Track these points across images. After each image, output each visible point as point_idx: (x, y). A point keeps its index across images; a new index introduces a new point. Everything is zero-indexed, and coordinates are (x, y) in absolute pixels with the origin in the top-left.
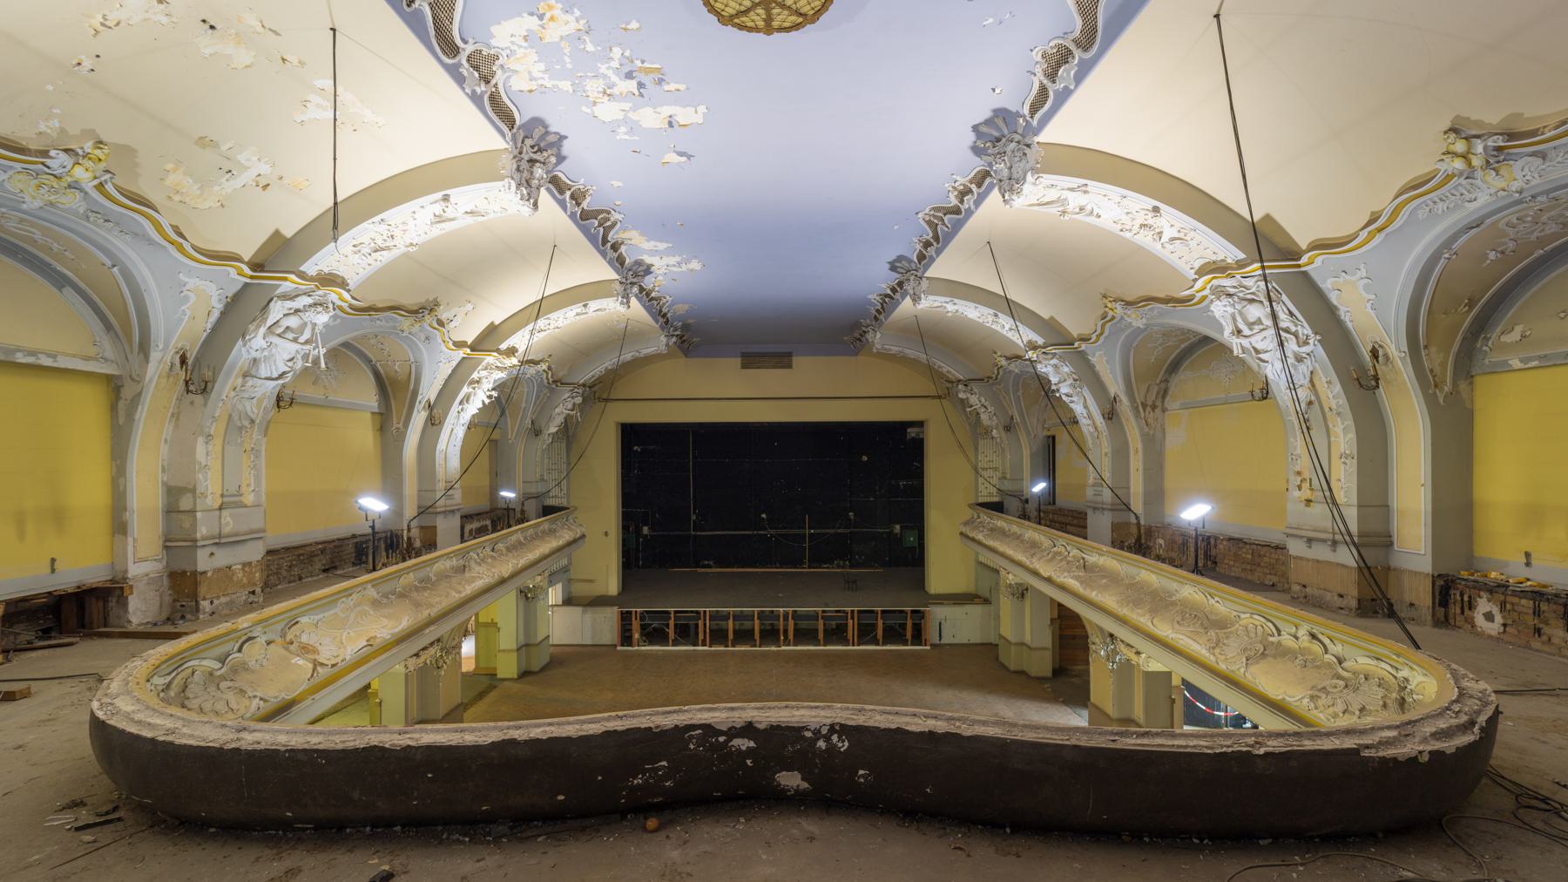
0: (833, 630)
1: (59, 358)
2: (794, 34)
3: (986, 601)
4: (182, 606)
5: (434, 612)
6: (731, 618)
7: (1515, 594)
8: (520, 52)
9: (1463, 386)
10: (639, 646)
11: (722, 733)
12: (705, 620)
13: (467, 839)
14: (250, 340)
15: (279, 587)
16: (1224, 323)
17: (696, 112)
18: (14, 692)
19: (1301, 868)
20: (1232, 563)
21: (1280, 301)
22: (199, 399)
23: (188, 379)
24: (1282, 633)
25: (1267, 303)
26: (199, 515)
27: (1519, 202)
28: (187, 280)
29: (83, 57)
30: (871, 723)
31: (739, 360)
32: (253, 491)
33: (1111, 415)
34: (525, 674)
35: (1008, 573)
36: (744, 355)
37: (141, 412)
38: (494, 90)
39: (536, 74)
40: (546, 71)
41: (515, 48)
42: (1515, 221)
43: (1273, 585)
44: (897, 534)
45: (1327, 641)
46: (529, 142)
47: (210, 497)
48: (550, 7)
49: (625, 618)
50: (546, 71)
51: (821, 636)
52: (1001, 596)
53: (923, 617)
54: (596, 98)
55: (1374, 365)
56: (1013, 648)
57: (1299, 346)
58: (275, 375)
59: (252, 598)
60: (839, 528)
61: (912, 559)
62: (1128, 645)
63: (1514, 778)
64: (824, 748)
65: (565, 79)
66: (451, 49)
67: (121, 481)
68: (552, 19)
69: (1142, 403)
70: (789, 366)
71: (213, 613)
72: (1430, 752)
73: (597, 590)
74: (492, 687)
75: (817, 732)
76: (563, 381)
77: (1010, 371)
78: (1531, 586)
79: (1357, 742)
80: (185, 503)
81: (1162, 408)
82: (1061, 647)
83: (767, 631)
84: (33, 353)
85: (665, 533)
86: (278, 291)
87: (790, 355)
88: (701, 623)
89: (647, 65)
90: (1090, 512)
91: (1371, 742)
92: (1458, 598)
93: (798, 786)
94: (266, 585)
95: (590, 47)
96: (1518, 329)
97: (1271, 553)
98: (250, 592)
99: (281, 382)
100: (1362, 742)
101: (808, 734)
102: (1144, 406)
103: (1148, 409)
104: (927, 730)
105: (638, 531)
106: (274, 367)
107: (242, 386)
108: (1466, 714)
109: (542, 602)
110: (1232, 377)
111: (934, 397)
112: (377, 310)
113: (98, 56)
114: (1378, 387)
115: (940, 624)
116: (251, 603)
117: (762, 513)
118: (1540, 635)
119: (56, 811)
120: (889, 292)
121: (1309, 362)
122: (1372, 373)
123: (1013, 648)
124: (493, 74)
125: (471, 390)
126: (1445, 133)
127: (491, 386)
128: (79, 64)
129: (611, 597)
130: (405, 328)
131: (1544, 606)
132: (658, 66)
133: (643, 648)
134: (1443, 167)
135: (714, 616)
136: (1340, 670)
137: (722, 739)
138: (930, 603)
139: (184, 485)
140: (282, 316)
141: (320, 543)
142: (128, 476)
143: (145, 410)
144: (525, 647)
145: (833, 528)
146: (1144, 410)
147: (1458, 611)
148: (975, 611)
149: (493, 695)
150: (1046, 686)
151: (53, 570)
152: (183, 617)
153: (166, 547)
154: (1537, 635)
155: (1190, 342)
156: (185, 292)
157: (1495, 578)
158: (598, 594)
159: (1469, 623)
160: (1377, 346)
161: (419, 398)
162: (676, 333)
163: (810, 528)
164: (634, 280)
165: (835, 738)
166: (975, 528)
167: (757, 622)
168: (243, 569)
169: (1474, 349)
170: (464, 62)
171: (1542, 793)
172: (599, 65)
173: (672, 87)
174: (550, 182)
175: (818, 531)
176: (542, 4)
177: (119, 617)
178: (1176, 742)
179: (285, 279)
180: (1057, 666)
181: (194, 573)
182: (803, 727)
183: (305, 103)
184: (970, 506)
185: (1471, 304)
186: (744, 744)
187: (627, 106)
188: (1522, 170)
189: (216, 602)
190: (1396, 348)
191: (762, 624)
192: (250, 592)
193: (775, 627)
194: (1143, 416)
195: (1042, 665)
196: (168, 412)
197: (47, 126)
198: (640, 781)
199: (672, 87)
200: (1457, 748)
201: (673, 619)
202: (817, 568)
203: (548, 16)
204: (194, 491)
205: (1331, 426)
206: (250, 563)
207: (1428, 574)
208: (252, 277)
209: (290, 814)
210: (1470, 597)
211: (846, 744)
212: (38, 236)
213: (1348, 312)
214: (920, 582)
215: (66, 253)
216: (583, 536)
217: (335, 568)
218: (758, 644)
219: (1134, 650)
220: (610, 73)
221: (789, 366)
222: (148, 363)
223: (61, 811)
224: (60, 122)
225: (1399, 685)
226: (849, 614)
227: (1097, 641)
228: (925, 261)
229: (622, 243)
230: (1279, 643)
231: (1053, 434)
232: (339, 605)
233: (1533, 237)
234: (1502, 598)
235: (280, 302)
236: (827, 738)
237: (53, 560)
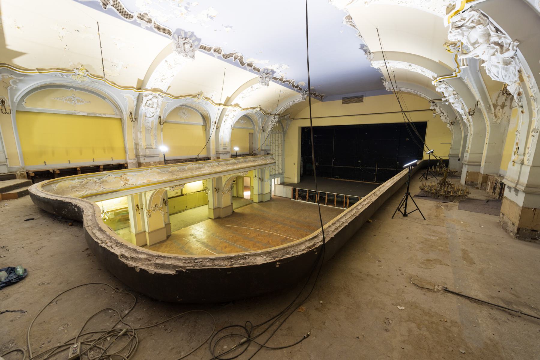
5: (178, 177)
10: (298, 200)
26: (140, 150)
28: (123, 94)
32: (155, 145)
34: (261, 202)
37: (125, 126)
38: (154, 24)
47: (142, 146)
49: (294, 190)
60: (391, 168)
69: (494, 105)
70: (362, 101)
73: (291, 181)
74: (251, 203)
76: (272, 113)
84: (100, 114)
86: (144, 95)
102: (495, 106)
124: (151, 19)
125: (226, 118)
129: (295, 184)
130: (196, 101)
141: (185, 159)
144: (261, 195)
146: (495, 109)
158: (291, 182)
161: (212, 121)
167: (335, 198)
170: (137, 19)
175: (382, 169)
194: (493, 113)
200: (155, 273)
206: (156, 162)
221: (362, 101)
232: (144, 172)
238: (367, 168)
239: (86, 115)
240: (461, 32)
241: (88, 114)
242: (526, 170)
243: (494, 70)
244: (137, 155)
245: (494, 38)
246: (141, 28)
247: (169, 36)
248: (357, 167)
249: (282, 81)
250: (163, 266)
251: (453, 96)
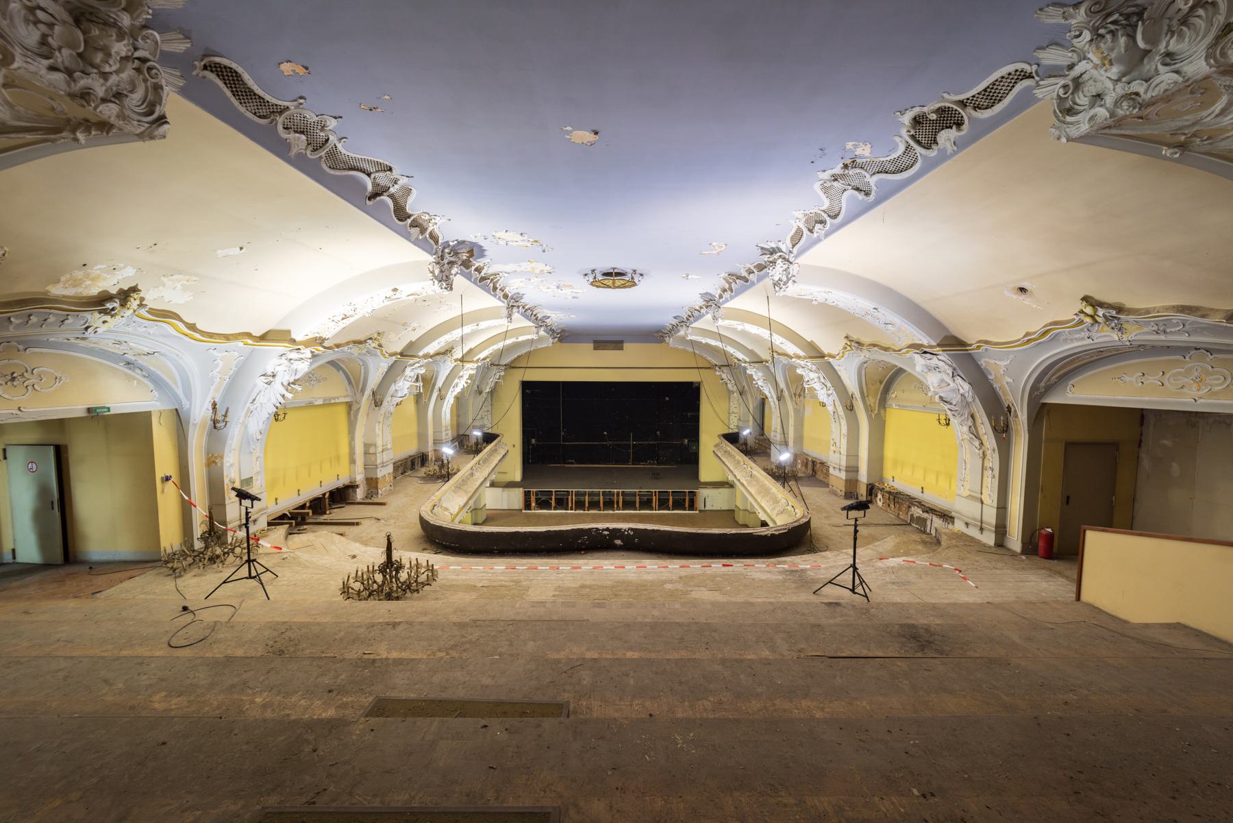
0: (645, 502)
9: (882, 411)
12: (572, 495)
33: (780, 398)
36: (595, 342)
51: (638, 505)
53: (695, 495)
56: (741, 512)
61: (690, 460)
67: (353, 443)
70: (621, 349)
75: (625, 530)
80: (372, 450)
83: (607, 502)
87: (622, 342)
88: (570, 498)
99: (401, 399)
102: (795, 395)
123: (741, 512)
127: (467, 377)
129: (517, 482)
135: (577, 494)
145: (647, 440)
148: (724, 491)
153: (365, 468)
163: (633, 441)
166: (719, 449)
167: (601, 497)
175: (638, 443)
177: (353, 496)
184: (719, 436)
185: (881, 382)
186: (606, 533)
190: (857, 395)
191: (604, 498)
216: (508, 451)
217: (405, 472)
221: (621, 349)
236: (628, 531)
237: (338, 475)
238: (618, 443)
239: (322, 403)
241: (325, 400)
242: (844, 458)
243: (822, 397)
244: (365, 465)
245: (822, 380)
249: (529, 313)
250: (778, 530)
251: (762, 380)
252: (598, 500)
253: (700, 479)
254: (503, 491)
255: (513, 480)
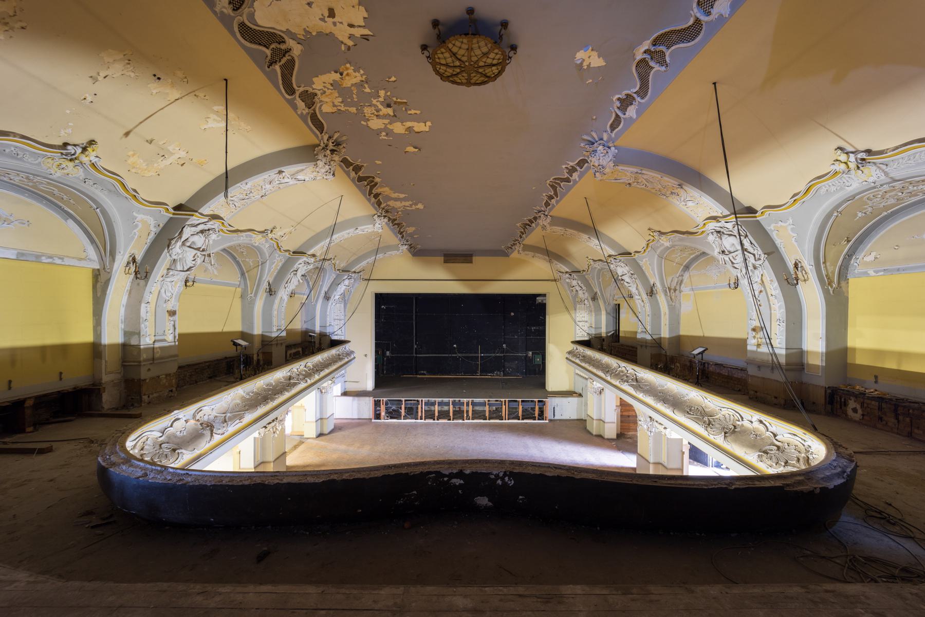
1: (65, 259)
2: (482, 87)
3: (580, 395)
4: (132, 399)
6: (437, 404)
7: (869, 398)
8: (328, 92)
11: (445, 476)
12: (422, 405)
13: (308, 533)
14: (172, 249)
15: (185, 387)
16: (715, 247)
17: (425, 125)
18: (44, 449)
19: (752, 549)
20: (716, 378)
21: (746, 236)
22: (142, 282)
23: (137, 271)
24: (744, 419)
25: (738, 237)
27: (874, 188)
28: (137, 215)
29: (87, 95)
30: (525, 471)
31: (442, 258)
34: (320, 435)
35: (593, 381)
39: (336, 103)
40: (342, 102)
41: (326, 89)
42: (872, 197)
43: (739, 390)
44: (530, 357)
45: (768, 425)
46: (331, 141)
48: (347, 69)
49: (377, 404)
50: (342, 102)
52: (589, 393)
54: (370, 117)
55: (796, 272)
57: (756, 261)
58: (186, 269)
59: (171, 394)
62: (660, 424)
63: (865, 500)
64: (500, 484)
65: (352, 107)
66: (291, 91)
68: (348, 75)
70: (471, 262)
71: (150, 402)
72: (820, 488)
74: (301, 443)
75: (497, 476)
77: (595, 268)
78: (878, 394)
79: (783, 483)
81: (680, 290)
82: (622, 422)
85: (399, 355)
87: (471, 256)
88: (420, 407)
89: (399, 100)
90: (639, 348)
91: (790, 482)
92: (839, 400)
93: (486, 504)
94: (178, 386)
95: (367, 90)
96: (873, 254)
97: (739, 373)
98: (169, 391)
100: (785, 483)
101: (493, 477)
102: (670, 289)
103: (672, 291)
104: (556, 475)
105: (384, 354)
106: (185, 264)
107: (167, 275)
108: (840, 467)
109: (330, 394)
110: (718, 275)
111: (552, 280)
112: (241, 231)
113: (95, 95)
114: (797, 284)
115: (554, 408)
116: (170, 397)
117: (454, 344)
118: (881, 421)
119: (79, 517)
120: (528, 222)
121: (761, 270)
122: (794, 276)
126: (836, 150)
128: (85, 99)
131: (884, 405)
132: (405, 101)
133: (387, 421)
134: (833, 167)
136: (775, 441)
137: (446, 479)
138: (549, 397)
139: (133, 331)
140: (189, 235)
141: (207, 362)
142: (102, 326)
143: (113, 288)
147: (839, 407)
148: (574, 400)
149: (302, 447)
150: (613, 443)
151: (61, 379)
152: (132, 405)
153: (124, 366)
154: (880, 421)
155: (695, 254)
156: (136, 223)
157: (858, 389)
159: (844, 414)
160: (797, 262)
162: (407, 243)
163: (481, 353)
164: (386, 215)
165: (507, 479)
167: (451, 406)
168: (166, 378)
169: (849, 264)
171: (879, 509)
172: (372, 99)
173: (413, 112)
174: (341, 162)
175: (486, 355)
176: (343, 67)
178: (688, 483)
179: (192, 215)
180: (619, 433)
181: (140, 380)
182: (489, 473)
183: (206, 119)
186: (457, 482)
187: (386, 121)
188: (876, 171)
189: (151, 396)
190: (808, 264)
192: (169, 391)
193: (461, 409)
195: (611, 431)
196: (125, 289)
197: (65, 133)
198: (402, 502)
199: (413, 112)
200: (835, 486)
201: (404, 404)
202: (485, 376)
203: (345, 73)
204: (139, 334)
205: (772, 304)
206: (170, 374)
207: (823, 387)
208: (174, 214)
209: (212, 520)
210: (845, 399)
211: (513, 482)
212: (56, 192)
213: (782, 242)
214: (543, 385)
215: (71, 201)
217: (216, 376)
218: (452, 419)
219: (663, 427)
220: (378, 104)
221: (471, 262)
222: (114, 262)
223: (81, 517)
224: (72, 130)
225: (806, 450)
226: (503, 403)
227: (642, 419)
228: (550, 207)
229: (380, 194)
230: (742, 425)
231: (619, 303)
233: (881, 205)
234: (862, 400)
235: (189, 228)
236: (503, 479)
240: (719, 235)
246: (294, 113)
247: (318, 133)
248: (453, 355)
252: (448, 410)
253: (546, 388)
254: (353, 400)
255: (364, 389)
